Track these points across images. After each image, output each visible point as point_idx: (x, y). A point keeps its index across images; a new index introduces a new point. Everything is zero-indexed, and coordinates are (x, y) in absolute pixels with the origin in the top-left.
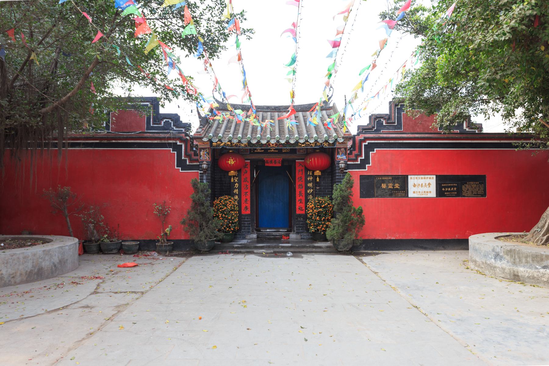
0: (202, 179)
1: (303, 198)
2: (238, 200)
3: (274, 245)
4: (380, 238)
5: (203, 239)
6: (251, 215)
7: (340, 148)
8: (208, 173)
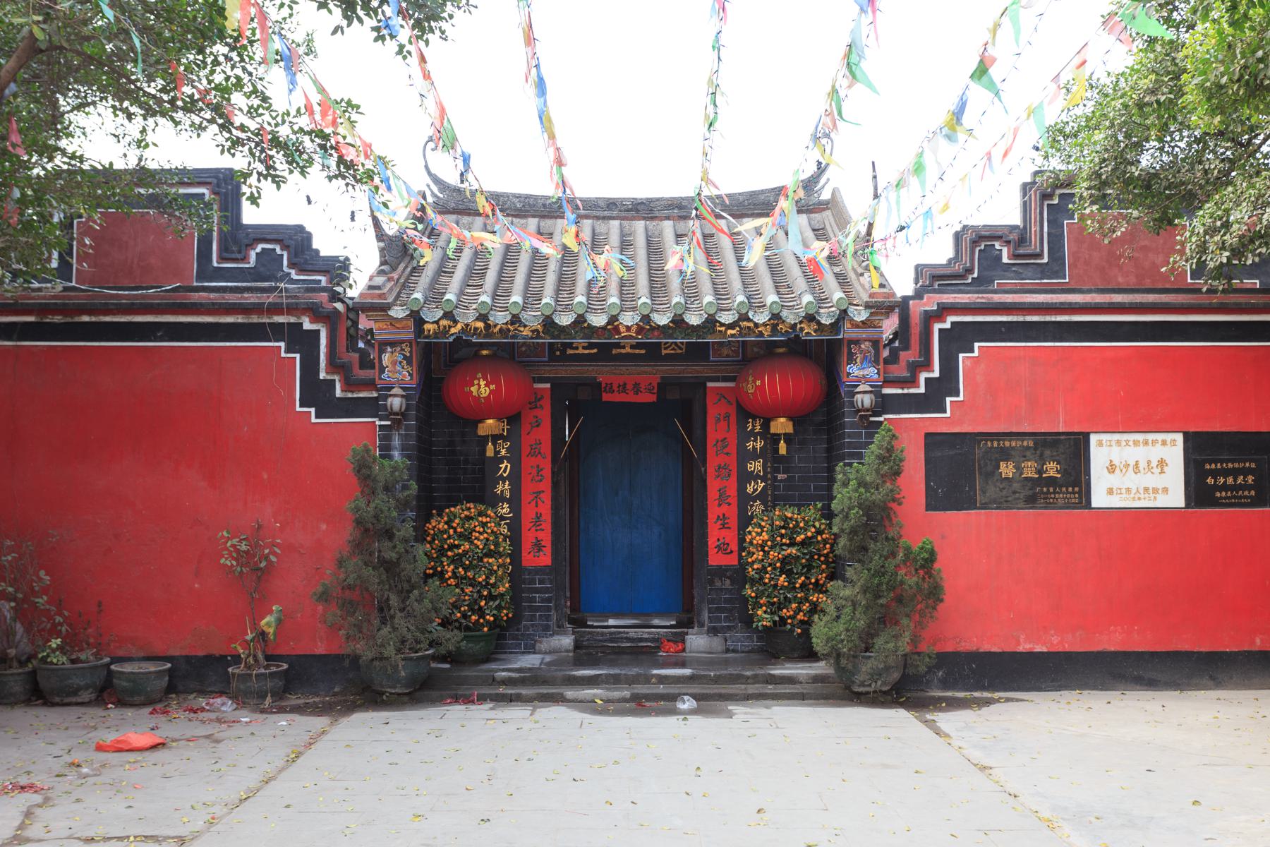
0: (386, 449)
1: (732, 512)
3: (634, 671)
4: (995, 649)
5: (390, 651)
6: (553, 569)
7: (857, 342)
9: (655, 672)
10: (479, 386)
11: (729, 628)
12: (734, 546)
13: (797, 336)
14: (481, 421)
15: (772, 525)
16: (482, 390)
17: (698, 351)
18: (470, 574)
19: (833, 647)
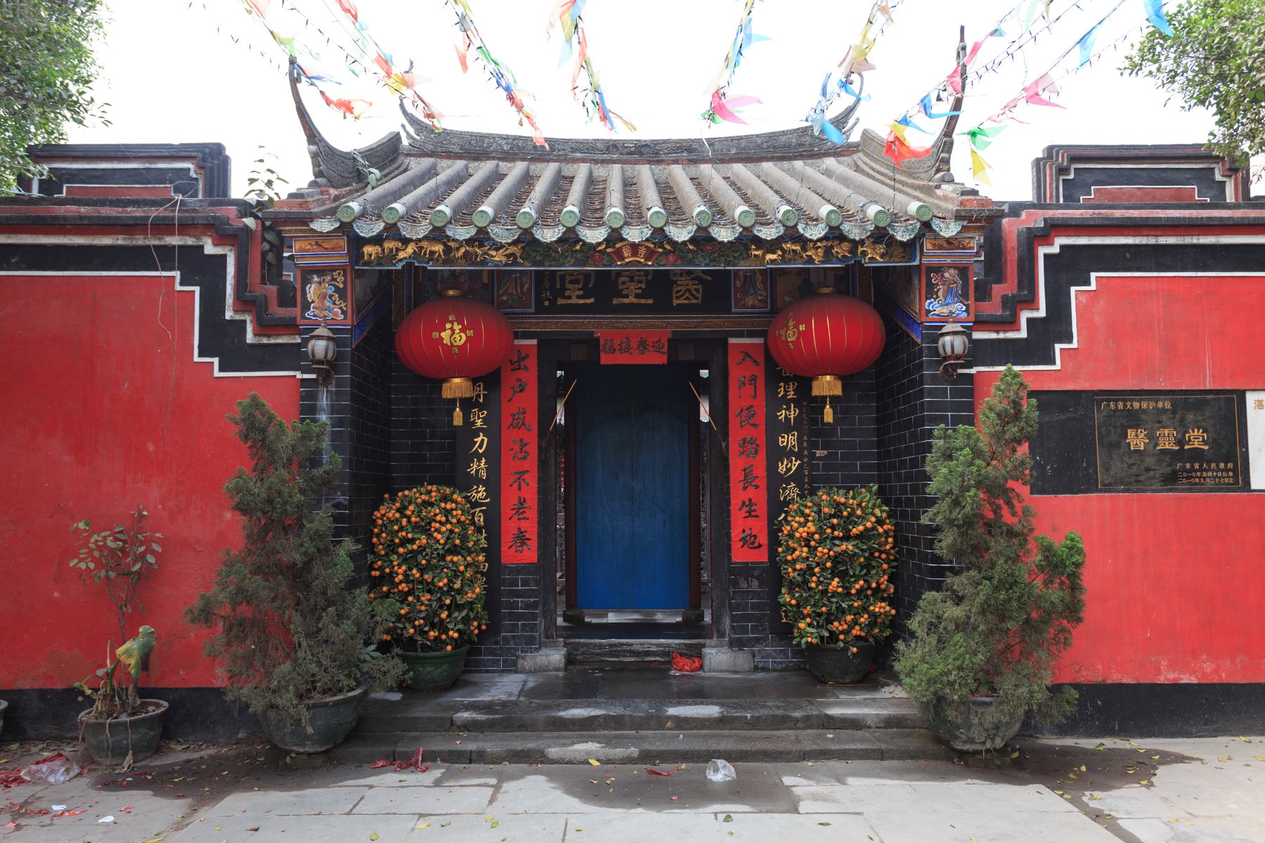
0: (309, 410)
1: (760, 498)
2: (481, 510)
3: (642, 708)
5: (286, 699)
6: (544, 566)
7: (938, 269)
8: (339, 383)
9: (672, 711)
10: (453, 330)
11: (757, 641)
12: (763, 539)
14: (446, 380)
15: (819, 512)
17: (717, 291)
18: (428, 577)
19: (935, 693)
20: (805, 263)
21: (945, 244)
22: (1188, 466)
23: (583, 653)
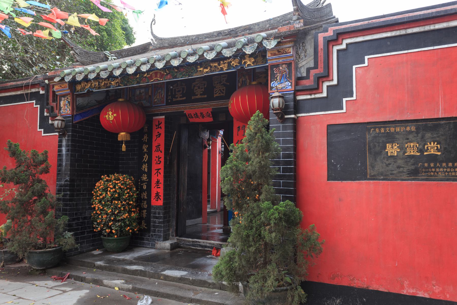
4: (381, 289)
7: (277, 66)
10: (109, 114)
13: (242, 68)
16: (110, 117)
20: (220, 71)
21: (277, 53)
22: (426, 165)
23: (183, 244)
